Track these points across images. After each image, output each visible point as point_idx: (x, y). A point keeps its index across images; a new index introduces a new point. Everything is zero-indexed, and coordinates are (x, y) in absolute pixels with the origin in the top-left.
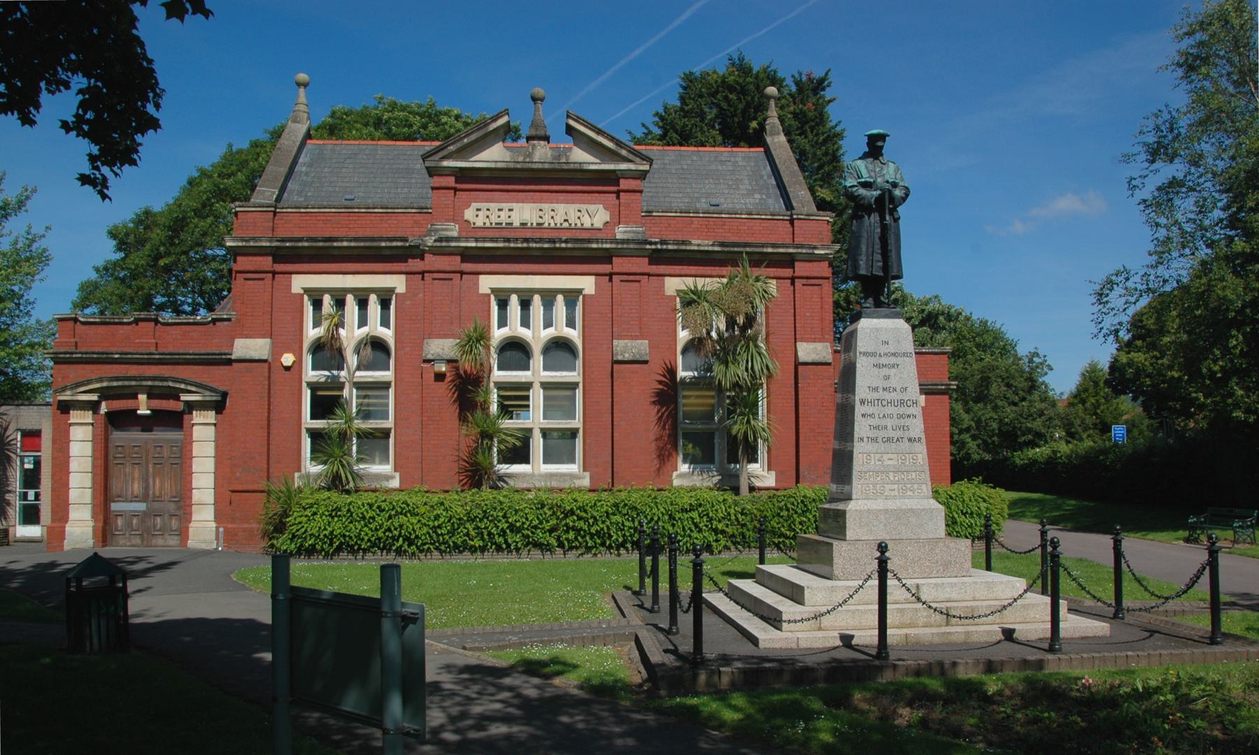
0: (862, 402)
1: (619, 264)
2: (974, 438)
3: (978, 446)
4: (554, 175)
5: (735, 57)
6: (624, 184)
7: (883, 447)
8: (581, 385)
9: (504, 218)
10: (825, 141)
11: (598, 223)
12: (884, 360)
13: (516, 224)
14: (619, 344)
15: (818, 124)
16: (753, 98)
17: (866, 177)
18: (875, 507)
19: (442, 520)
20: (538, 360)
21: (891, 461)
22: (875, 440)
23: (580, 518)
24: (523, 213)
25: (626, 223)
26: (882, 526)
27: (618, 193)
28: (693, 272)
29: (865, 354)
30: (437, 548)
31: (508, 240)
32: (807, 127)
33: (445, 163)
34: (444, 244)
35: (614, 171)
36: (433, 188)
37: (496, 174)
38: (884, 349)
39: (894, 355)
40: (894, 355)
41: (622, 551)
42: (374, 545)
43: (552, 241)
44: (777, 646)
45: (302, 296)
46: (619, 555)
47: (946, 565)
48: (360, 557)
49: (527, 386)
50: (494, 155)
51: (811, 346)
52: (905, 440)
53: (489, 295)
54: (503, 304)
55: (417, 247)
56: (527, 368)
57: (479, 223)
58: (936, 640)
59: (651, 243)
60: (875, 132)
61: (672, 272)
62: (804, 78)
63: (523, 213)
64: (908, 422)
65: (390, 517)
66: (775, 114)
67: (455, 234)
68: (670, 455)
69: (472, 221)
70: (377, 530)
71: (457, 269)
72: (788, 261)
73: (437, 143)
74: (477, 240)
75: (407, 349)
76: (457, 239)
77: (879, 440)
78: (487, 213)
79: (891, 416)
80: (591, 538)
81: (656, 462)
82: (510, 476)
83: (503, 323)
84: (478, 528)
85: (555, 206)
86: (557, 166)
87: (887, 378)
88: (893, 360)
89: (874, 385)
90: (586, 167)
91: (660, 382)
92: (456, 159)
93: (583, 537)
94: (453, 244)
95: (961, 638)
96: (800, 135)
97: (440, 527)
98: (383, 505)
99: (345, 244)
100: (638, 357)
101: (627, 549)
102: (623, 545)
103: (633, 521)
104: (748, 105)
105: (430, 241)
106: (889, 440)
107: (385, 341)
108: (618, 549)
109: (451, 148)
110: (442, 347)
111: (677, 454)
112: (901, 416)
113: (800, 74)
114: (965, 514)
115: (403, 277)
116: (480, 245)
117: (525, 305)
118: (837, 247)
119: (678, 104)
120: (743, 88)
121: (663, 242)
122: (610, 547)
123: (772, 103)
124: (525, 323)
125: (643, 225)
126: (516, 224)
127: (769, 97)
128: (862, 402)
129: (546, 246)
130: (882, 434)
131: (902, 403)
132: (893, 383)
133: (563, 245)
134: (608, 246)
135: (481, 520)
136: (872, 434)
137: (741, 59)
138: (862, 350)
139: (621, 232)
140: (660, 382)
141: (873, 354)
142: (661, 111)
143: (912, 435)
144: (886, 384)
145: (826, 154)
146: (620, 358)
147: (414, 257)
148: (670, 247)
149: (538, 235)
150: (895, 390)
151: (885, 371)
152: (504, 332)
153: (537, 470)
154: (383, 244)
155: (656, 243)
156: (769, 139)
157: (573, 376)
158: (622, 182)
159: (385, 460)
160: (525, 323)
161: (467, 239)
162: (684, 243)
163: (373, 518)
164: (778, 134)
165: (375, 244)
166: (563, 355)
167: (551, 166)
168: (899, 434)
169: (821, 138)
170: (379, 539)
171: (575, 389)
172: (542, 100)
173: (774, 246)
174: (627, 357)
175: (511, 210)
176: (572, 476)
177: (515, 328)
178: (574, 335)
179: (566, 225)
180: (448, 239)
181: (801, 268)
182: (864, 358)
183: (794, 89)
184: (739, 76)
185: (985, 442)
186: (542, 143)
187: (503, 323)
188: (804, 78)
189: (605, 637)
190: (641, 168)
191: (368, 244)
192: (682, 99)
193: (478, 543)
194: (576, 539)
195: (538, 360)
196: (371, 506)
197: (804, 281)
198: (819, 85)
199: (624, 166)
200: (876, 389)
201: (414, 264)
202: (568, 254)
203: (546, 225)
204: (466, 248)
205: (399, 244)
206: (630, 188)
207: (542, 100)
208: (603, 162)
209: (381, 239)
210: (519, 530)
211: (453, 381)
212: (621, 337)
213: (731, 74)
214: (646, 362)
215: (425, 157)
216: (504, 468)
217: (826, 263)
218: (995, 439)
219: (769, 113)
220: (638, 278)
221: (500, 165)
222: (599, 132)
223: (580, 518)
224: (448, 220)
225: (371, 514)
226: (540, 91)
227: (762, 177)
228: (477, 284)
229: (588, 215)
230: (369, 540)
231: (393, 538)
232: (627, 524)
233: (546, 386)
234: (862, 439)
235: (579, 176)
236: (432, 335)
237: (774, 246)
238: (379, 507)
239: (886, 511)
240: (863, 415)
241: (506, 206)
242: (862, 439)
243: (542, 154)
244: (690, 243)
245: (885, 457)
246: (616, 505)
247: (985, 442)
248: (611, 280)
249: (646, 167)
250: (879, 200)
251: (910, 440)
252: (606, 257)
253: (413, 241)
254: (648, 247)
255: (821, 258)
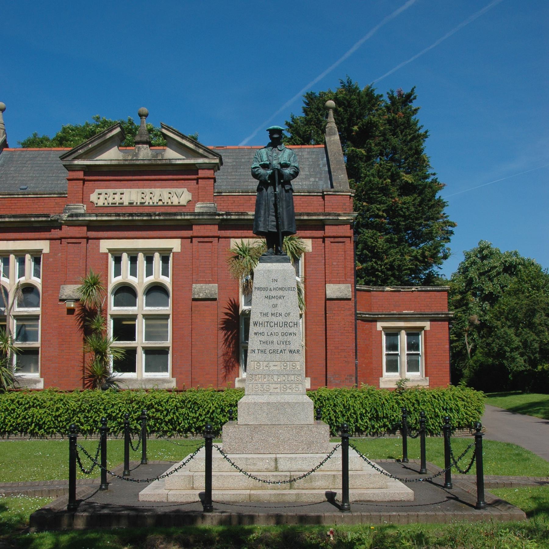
0: (255, 324)
1: (197, 230)
2: (522, 355)
3: (525, 361)
4: (128, 169)
5: (345, 81)
6: (202, 173)
7: (269, 356)
8: (171, 316)
9: (117, 200)
10: (412, 140)
11: (183, 202)
12: (273, 293)
13: (126, 203)
14: (196, 287)
15: (406, 128)
16: (355, 110)
17: (265, 161)
18: (261, 401)
19: (61, 411)
20: (141, 299)
21: (276, 367)
22: (263, 351)
23: (157, 410)
24: (131, 195)
25: (203, 201)
26: (265, 415)
27: (197, 180)
28: (239, 235)
29: (259, 289)
30: (59, 431)
31: (118, 215)
32: (398, 130)
33: (76, 162)
34: (74, 218)
35: (194, 164)
36: (69, 180)
37: (112, 169)
38: (273, 285)
39: (281, 289)
40: (281, 289)
41: (189, 434)
42: (16, 429)
43: (149, 215)
44: (152, 499)
45: (107, 254)
46: (186, 437)
47: (310, 444)
48: (6, 437)
49: (133, 317)
50: (112, 155)
51: (337, 286)
52: (287, 351)
53: (107, 254)
54: (118, 260)
55: (56, 221)
56: (135, 305)
57: (100, 203)
58: (273, 499)
59: (219, 215)
60: (276, 127)
61: (236, 235)
62: (396, 94)
63: (131, 195)
64: (289, 338)
65: (26, 409)
66: (333, 120)
67: (82, 211)
68: (233, 366)
69: (95, 202)
70: (17, 418)
71: (84, 235)
72: (320, 225)
73: (69, 149)
74: (97, 216)
75: (50, 292)
76: (83, 215)
77: (267, 352)
78: (104, 196)
79: (277, 334)
80: (166, 425)
81: (223, 371)
82: (120, 381)
83: (118, 273)
84: (87, 417)
85: (153, 190)
86: (153, 162)
87: (275, 306)
88: (280, 293)
89: (265, 311)
90: (174, 162)
91: (226, 314)
92: (84, 159)
93: (160, 424)
94: (81, 219)
95: (293, 499)
96: (393, 135)
97: (59, 416)
98: (21, 400)
99: (7, 220)
100: (209, 296)
101: (192, 433)
102: (189, 430)
103: (196, 413)
104: (352, 115)
105: (65, 217)
106: (274, 351)
107: (36, 287)
108: (186, 433)
109: (81, 151)
110: (70, 290)
111: (239, 365)
112: (284, 334)
113: (392, 92)
114: (446, 410)
115: (48, 242)
116: (99, 218)
117: (133, 260)
118: (356, 214)
119: (303, 115)
120: (349, 102)
121: (227, 214)
122: (179, 431)
123: (331, 112)
124: (133, 273)
125: (214, 202)
126: (126, 203)
127: (328, 108)
128: (255, 324)
129: (145, 218)
130: (269, 347)
131: (286, 324)
132: (280, 309)
133: (157, 218)
134: (189, 217)
135: (89, 412)
136: (261, 347)
137: (349, 82)
138: (257, 286)
139: (199, 207)
140: (226, 314)
141: (265, 289)
142: (290, 121)
143: (293, 348)
144: (274, 311)
145: (410, 149)
146: (196, 297)
147: (55, 228)
148: (233, 217)
149: (140, 211)
150: (280, 315)
151: (274, 301)
152: (119, 279)
153: (141, 376)
154: (33, 219)
155: (222, 215)
156: (327, 139)
157: (167, 310)
158: (200, 171)
159: (36, 370)
160: (133, 273)
161: (90, 215)
162: (243, 214)
163: (14, 410)
164: (335, 134)
165: (27, 219)
166: (158, 295)
167: (150, 162)
168: (283, 347)
169: (409, 137)
170: (19, 424)
171: (167, 319)
172: (146, 116)
173: (308, 214)
174: (202, 296)
175: (122, 194)
176: (164, 381)
177: (126, 277)
178: (167, 281)
179: (160, 203)
180: (77, 215)
181: (330, 230)
182: (258, 292)
183: (389, 102)
184: (346, 95)
185: (529, 358)
186: (145, 146)
187: (118, 273)
188: (396, 94)
189: (42, 491)
190: (213, 161)
191: (22, 219)
192: (305, 111)
193: (86, 427)
194: (155, 425)
195: (141, 299)
196: (13, 401)
197: (332, 240)
198: (408, 98)
199: (201, 161)
200: (266, 315)
201: (56, 233)
202: (162, 223)
203: (147, 204)
204: (90, 221)
205: (44, 219)
206: (206, 176)
207: (146, 116)
208: (188, 158)
209: (31, 216)
210: (115, 419)
211: (78, 314)
212: (198, 282)
213: (341, 92)
214: (215, 299)
215: (63, 158)
216: (118, 375)
217: (348, 227)
218: (537, 355)
219: (329, 120)
220: (210, 240)
221: (114, 163)
222: (183, 137)
223: (157, 410)
224: (78, 202)
225: (13, 406)
226: (144, 110)
227: (319, 165)
228: (98, 246)
229: (175, 196)
230: (11, 425)
231: (27, 423)
232: (191, 414)
233: (147, 317)
234: (254, 351)
235: (170, 168)
236: (66, 282)
237: (308, 214)
238: (18, 402)
239: (268, 403)
240: (256, 334)
241: (119, 191)
242: (254, 351)
243: (144, 153)
244: (247, 214)
245: (271, 364)
246: (183, 402)
247: (529, 358)
248: (324, 242)
249: (217, 161)
250: (272, 176)
251: (291, 351)
252: (188, 225)
253: (53, 217)
254: (217, 217)
255: (344, 223)
